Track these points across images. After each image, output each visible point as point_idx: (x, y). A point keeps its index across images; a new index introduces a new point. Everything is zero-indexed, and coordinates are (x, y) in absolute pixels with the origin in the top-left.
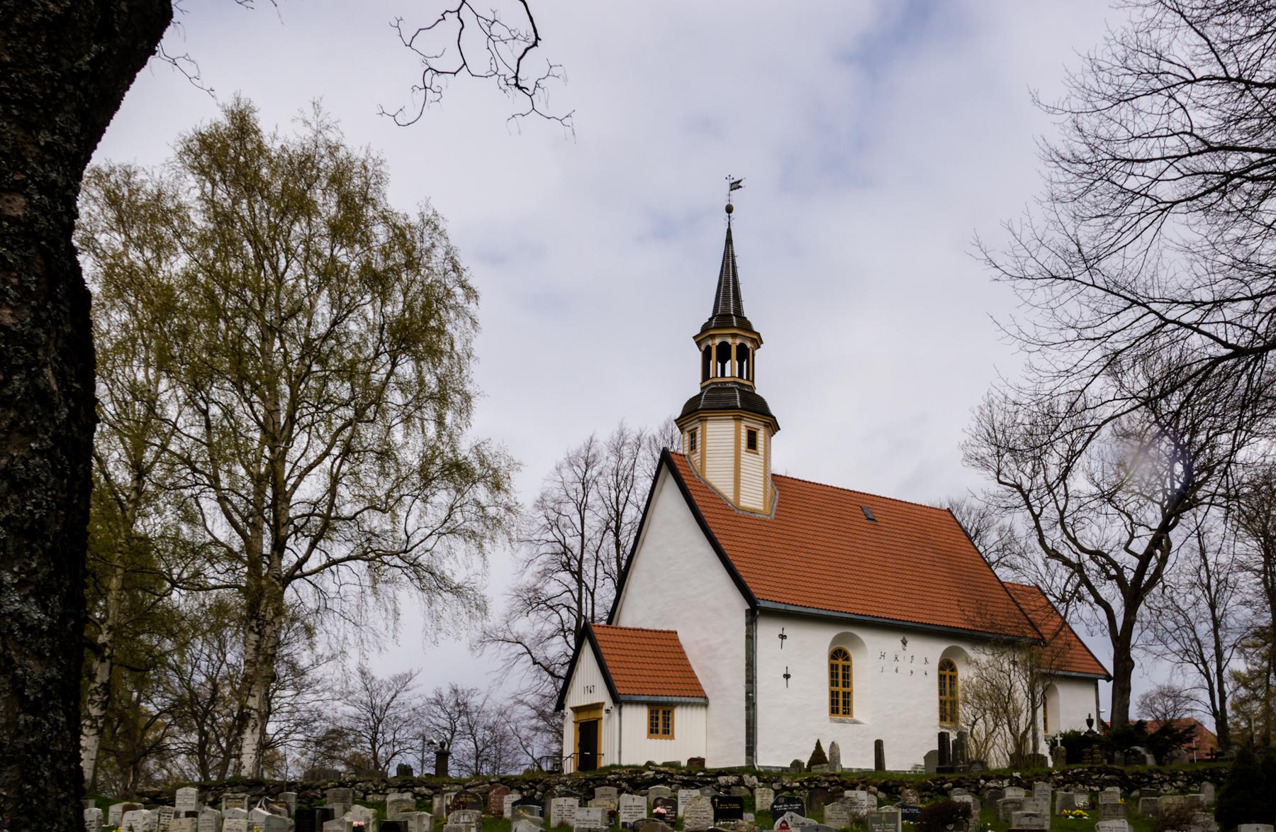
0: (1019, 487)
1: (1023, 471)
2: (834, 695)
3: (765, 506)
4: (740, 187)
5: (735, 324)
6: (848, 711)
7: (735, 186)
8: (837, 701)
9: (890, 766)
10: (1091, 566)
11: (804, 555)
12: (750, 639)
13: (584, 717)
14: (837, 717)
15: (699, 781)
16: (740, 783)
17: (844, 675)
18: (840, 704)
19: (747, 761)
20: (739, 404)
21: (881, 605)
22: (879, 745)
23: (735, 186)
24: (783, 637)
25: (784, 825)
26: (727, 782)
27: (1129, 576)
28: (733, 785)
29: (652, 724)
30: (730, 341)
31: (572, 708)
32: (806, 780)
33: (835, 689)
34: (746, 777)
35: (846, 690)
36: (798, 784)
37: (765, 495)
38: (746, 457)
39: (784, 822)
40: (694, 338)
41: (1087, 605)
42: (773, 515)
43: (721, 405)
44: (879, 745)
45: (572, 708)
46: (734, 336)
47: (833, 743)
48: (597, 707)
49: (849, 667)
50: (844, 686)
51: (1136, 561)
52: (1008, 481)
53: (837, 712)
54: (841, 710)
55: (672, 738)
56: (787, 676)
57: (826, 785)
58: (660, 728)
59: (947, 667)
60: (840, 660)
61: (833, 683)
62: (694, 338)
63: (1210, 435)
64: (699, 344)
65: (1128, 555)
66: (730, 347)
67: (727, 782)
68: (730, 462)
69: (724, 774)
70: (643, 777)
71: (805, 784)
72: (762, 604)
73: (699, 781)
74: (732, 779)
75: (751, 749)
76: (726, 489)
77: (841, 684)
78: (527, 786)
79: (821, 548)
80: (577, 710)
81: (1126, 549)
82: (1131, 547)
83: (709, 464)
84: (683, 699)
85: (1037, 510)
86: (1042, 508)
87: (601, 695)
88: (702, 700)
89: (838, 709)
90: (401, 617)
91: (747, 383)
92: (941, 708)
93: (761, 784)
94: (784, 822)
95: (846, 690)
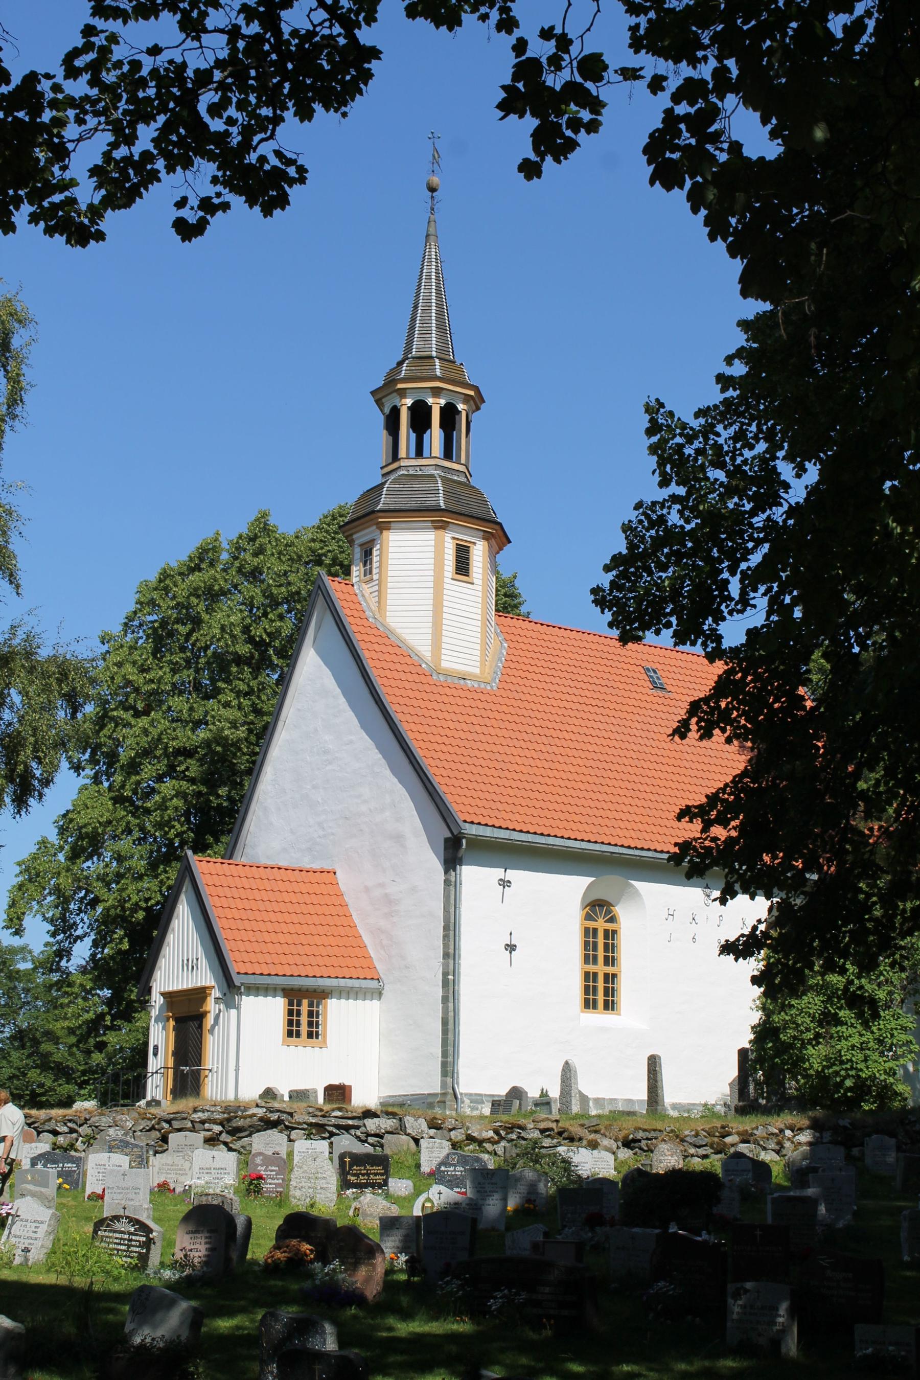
2: (589, 977)
6: (610, 1006)
8: (595, 988)
9: (671, 1096)
12: (451, 888)
16: (401, 1129)
17: (606, 946)
19: (444, 1085)
22: (653, 1064)
24: (504, 883)
31: (162, 994)
33: (591, 968)
36: (491, 1134)
38: (453, 588)
40: (372, 393)
41: (222, 1146)
43: (413, 505)
44: (653, 1064)
45: (162, 994)
46: (436, 392)
47: (567, 1063)
48: (200, 994)
49: (614, 932)
50: (606, 963)
53: (595, 1007)
54: (601, 1004)
56: (511, 948)
58: (304, 1029)
61: (589, 958)
62: (372, 393)
64: (379, 403)
66: (430, 408)
71: (503, 1133)
74: (386, 1123)
75: (448, 1068)
77: (601, 959)
78: (66, 1129)
80: (169, 996)
83: (393, 598)
87: (204, 977)
88: (374, 984)
89: (595, 1001)
90: (483, 406)
92: (562, 1075)
93: (432, 1132)
95: (610, 970)
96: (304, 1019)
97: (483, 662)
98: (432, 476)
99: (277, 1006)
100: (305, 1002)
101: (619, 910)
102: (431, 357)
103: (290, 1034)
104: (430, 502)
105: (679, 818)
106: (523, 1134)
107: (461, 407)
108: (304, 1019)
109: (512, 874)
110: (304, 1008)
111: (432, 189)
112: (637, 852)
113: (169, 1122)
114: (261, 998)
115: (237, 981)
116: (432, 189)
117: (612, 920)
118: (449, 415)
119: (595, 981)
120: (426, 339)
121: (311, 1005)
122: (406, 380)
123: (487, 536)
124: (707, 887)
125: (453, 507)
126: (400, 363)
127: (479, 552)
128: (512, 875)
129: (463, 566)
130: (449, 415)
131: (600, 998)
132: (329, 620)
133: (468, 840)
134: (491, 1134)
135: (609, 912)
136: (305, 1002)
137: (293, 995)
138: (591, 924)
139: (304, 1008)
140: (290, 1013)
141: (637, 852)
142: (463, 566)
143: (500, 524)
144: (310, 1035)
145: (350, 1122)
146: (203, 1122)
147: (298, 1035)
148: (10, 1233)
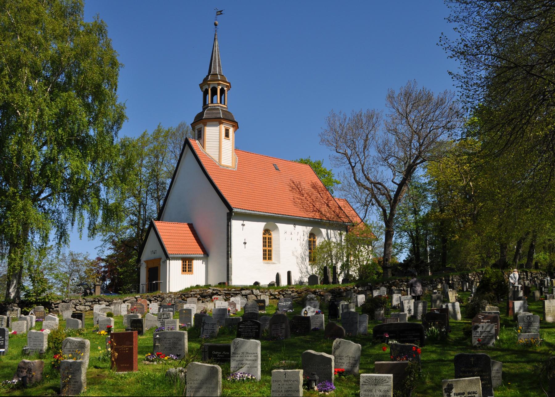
0: (345, 154)
1: (449, 157)
3: (232, 164)
4: (222, 14)
5: (219, 78)
6: (270, 259)
7: (219, 13)
10: (376, 190)
11: (251, 187)
13: (151, 266)
14: (266, 261)
15: (233, 293)
18: (267, 255)
20: (221, 116)
21: (285, 209)
23: (220, 13)
24: (243, 225)
25: (306, 312)
26: (246, 293)
27: (392, 194)
28: (248, 294)
29: (183, 268)
30: (216, 86)
32: (281, 291)
34: (254, 291)
35: (270, 248)
37: (232, 159)
38: (224, 141)
39: (306, 311)
42: (236, 169)
43: (213, 117)
50: (269, 247)
51: (397, 186)
52: (341, 151)
53: (266, 259)
55: (192, 274)
56: (245, 243)
57: (290, 292)
58: (187, 269)
59: (312, 235)
60: (267, 235)
63: (431, 129)
64: (201, 88)
65: (393, 183)
67: (246, 293)
68: (217, 144)
69: (244, 290)
70: (207, 292)
71: (281, 292)
72: (235, 210)
73: (233, 293)
76: (215, 157)
77: (267, 246)
78: (153, 299)
79: (258, 183)
81: (392, 181)
82: (395, 181)
84: (197, 255)
85: (353, 165)
86: (356, 163)
91: (224, 106)
94: (306, 311)
95: (270, 248)
96: (187, 266)
97: (232, 163)
98: (218, 109)
99: (179, 263)
100: (187, 261)
101: (272, 233)
102: (217, 74)
103: (183, 271)
104: (218, 116)
105: (81, 239)
106: (287, 293)
107: (225, 89)
108: (187, 266)
109: (245, 222)
110: (187, 263)
111: (216, 25)
112: (277, 215)
113: (184, 295)
114: (175, 261)
115: (170, 256)
116: (216, 25)
117: (270, 234)
118: (222, 91)
119: (266, 252)
120: (215, 69)
121: (189, 262)
122: (210, 81)
123: (233, 126)
124: (295, 224)
125: (224, 117)
126: (208, 76)
127: (231, 130)
128: (246, 223)
129: (227, 135)
130: (222, 91)
131: (267, 256)
132: (190, 151)
133: (234, 213)
134: (277, 293)
135: (269, 232)
136: (187, 261)
137: (184, 260)
138: (265, 236)
139: (187, 263)
140: (183, 265)
141: (277, 215)
142: (227, 135)
143: (237, 123)
144: (189, 271)
145: (237, 292)
146: (194, 295)
147: (186, 271)
148: (203, 329)
